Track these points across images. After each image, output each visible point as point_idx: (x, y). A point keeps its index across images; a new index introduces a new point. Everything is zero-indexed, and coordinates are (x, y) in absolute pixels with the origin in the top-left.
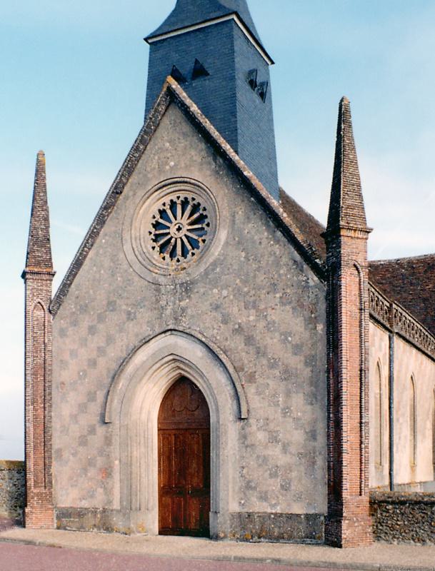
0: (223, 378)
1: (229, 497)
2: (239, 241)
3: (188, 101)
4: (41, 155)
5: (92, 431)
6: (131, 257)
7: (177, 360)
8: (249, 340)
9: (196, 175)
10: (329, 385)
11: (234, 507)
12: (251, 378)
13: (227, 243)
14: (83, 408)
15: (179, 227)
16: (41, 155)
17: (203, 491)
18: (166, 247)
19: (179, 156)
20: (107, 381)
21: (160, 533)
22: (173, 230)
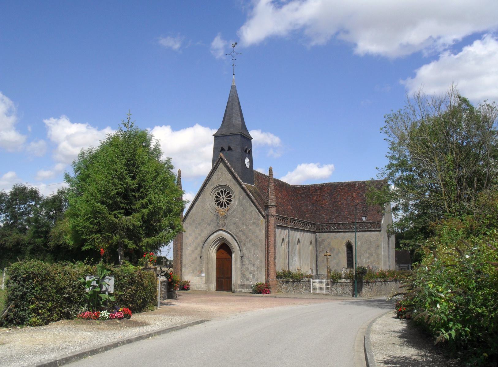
0: (236, 244)
1: (236, 278)
2: (241, 205)
3: (227, 162)
4: (233, 88)
5: (196, 259)
6: (209, 206)
7: (222, 239)
8: (244, 234)
9: (228, 184)
10: (275, 249)
11: (239, 282)
12: (244, 244)
13: (238, 205)
14: (193, 252)
15: (223, 198)
16: (233, 88)
17: (230, 278)
18: (220, 204)
19: (224, 177)
20: (202, 244)
21: (217, 290)
22: (221, 199)
